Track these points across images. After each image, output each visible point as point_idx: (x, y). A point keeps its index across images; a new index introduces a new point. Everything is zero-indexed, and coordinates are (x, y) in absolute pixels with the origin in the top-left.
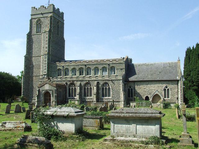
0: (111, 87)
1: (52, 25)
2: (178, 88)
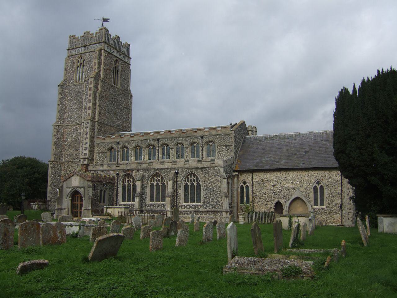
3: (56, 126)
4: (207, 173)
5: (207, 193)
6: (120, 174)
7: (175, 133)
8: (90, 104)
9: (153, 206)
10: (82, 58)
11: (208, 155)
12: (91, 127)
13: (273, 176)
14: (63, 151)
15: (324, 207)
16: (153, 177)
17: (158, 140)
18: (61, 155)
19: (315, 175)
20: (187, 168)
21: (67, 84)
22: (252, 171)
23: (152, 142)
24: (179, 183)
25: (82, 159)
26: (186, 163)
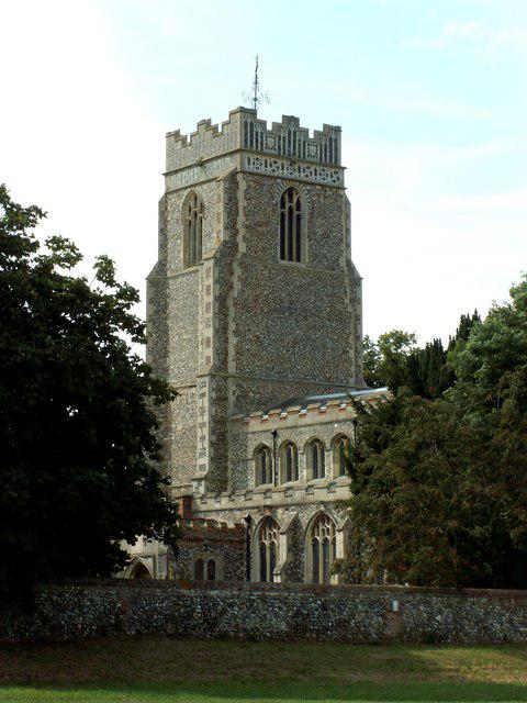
12: (214, 394)
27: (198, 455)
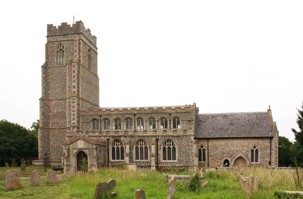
0: (176, 147)
1: (81, 53)
2: (271, 149)
3: (43, 100)
4: (181, 140)
5: (181, 153)
6: (110, 139)
7: (149, 110)
8: (75, 84)
9: (139, 163)
10: (61, 45)
11: (105, 128)
13: (223, 142)
14: (50, 120)
15: (258, 163)
16: (138, 142)
17: (135, 115)
18: (48, 123)
19: (253, 142)
20: (165, 136)
21: (49, 66)
22: (208, 139)
23: (130, 116)
24: (159, 146)
25: (71, 127)
26: (144, 132)
27: (72, 120)
